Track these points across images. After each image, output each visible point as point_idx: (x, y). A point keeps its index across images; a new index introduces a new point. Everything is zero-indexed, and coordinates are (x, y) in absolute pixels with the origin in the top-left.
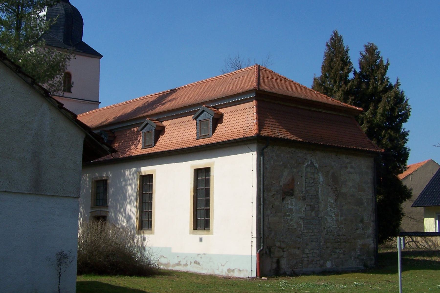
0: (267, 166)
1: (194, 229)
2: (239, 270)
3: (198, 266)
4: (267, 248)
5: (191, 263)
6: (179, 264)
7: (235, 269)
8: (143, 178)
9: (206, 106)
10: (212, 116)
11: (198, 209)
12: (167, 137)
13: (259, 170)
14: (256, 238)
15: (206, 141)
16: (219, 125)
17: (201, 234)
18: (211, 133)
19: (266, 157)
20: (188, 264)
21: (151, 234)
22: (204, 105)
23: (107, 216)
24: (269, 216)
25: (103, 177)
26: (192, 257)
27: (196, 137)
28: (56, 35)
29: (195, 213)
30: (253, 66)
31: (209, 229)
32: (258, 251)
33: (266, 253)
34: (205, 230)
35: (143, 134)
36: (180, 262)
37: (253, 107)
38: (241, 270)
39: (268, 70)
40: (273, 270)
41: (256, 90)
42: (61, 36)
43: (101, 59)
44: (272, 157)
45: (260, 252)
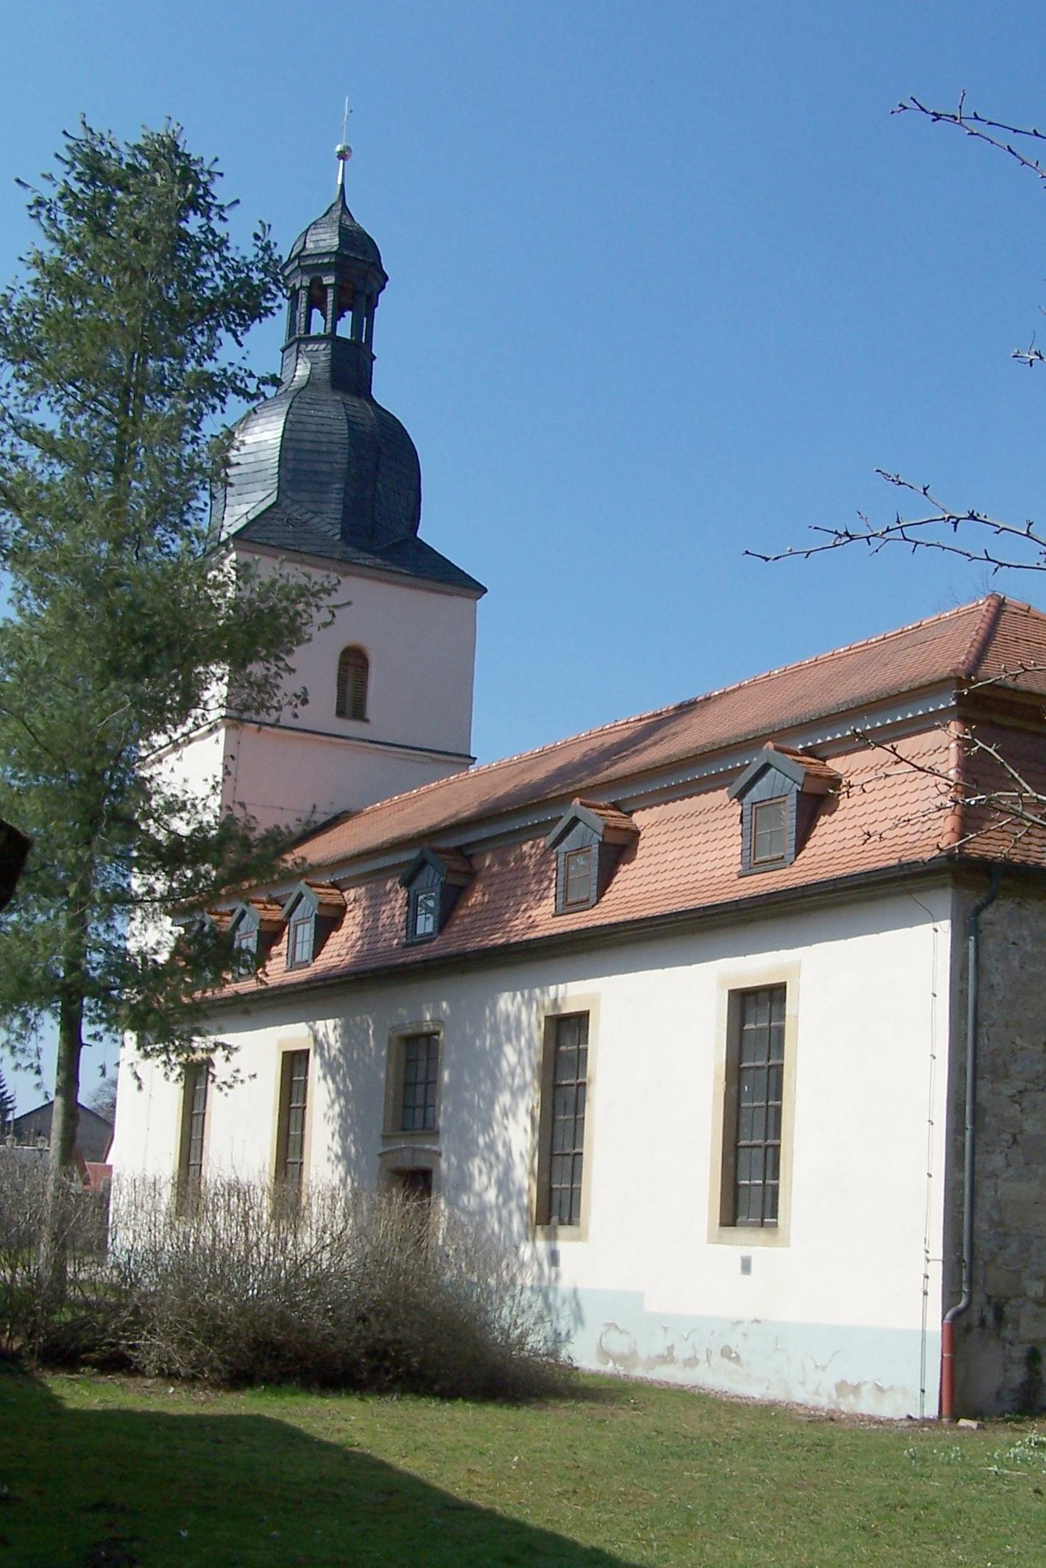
0: (996, 979)
1: (723, 1224)
2: (879, 1388)
3: (732, 1365)
4: (989, 1303)
5: (709, 1352)
6: (667, 1358)
7: (865, 1383)
8: (558, 1029)
9: (776, 749)
10: (796, 785)
11: (742, 1147)
12: (645, 871)
13: (961, 992)
14: (941, 1263)
15: (771, 881)
16: (823, 819)
17: (747, 1242)
18: (793, 849)
19: (990, 945)
20: (698, 1357)
21: (578, 1238)
22: (770, 745)
23: (434, 1170)
24: (997, 1177)
25: (421, 1022)
26: (712, 1333)
27: (740, 867)
28: (316, 513)
29: (731, 1160)
30: (981, 602)
31: (776, 1225)
32: (949, 1315)
33: (983, 1323)
34: (762, 1226)
35: (561, 858)
36: (671, 1349)
37: (947, 748)
38: (885, 1387)
39: (1037, 616)
40: (1011, 1390)
41: (960, 678)
42: (332, 516)
43: (478, 601)
44: (1014, 944)
45: (954, 1318)
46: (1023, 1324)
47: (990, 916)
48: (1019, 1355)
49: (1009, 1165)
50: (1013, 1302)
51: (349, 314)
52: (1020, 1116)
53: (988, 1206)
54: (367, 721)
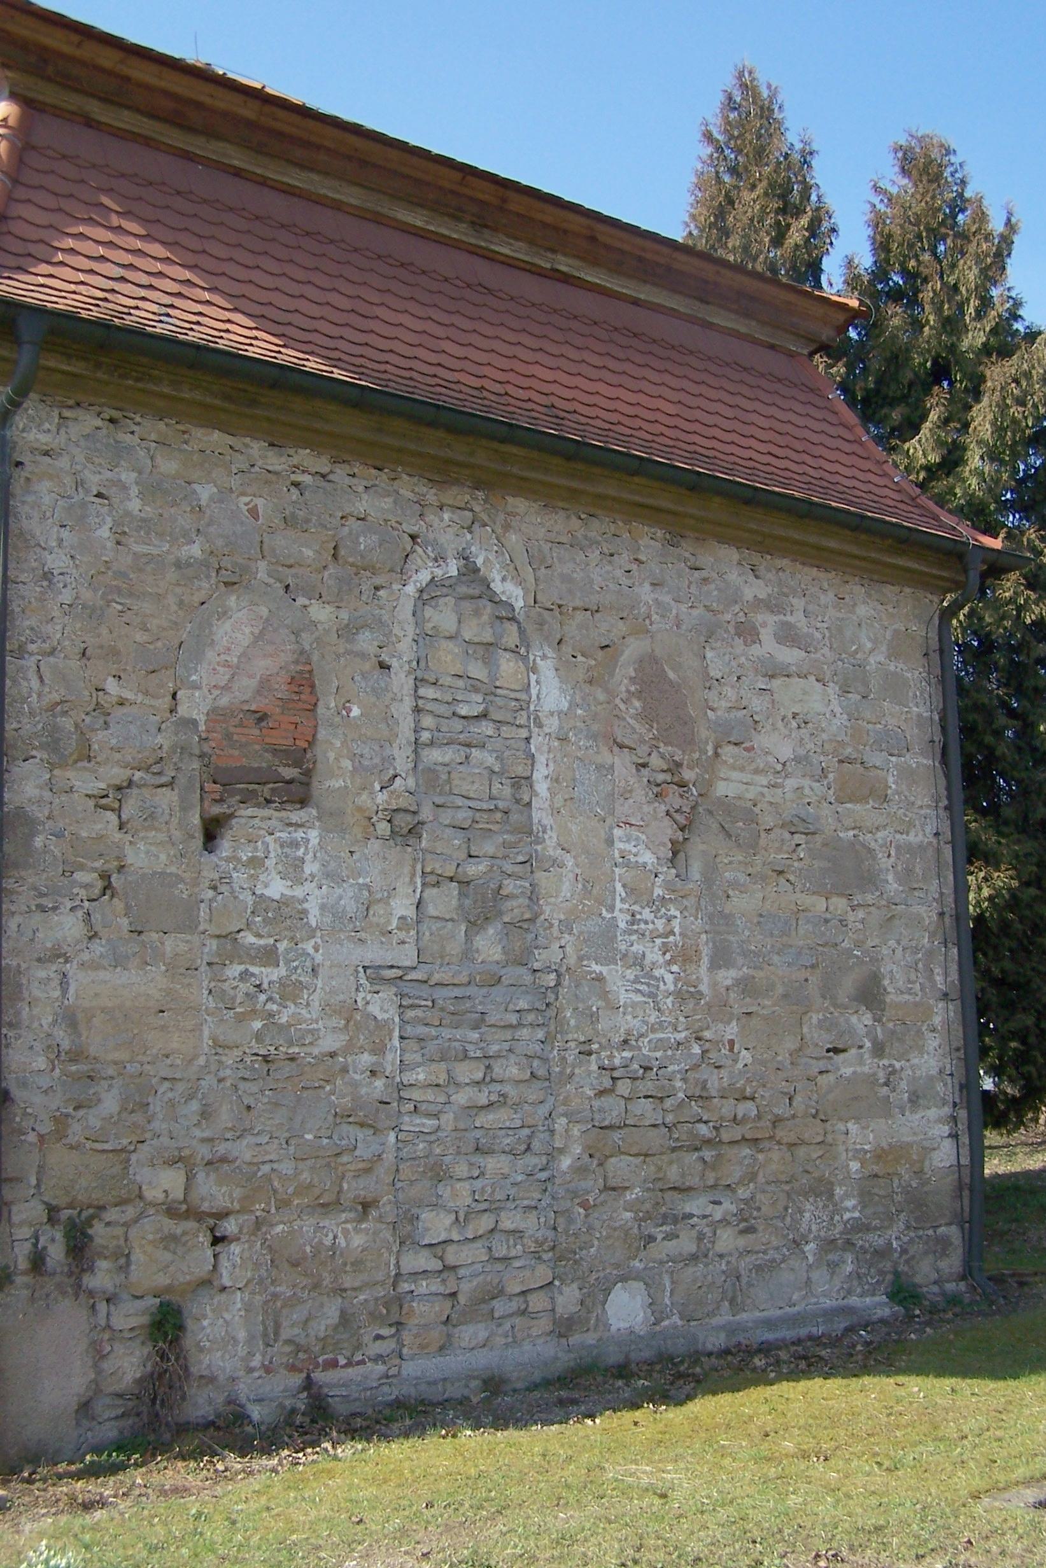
4: (52, 1220)
33: (38, 1262)
44: (99, 495)
46: (137, 1256)
47: (44, 438)
48: (134, 1322)
49: (93, 936)
50: (112, 1214)
51: (830, 865)
52: (118, 836)
53: (47, 1020)
54: (748, 87)
